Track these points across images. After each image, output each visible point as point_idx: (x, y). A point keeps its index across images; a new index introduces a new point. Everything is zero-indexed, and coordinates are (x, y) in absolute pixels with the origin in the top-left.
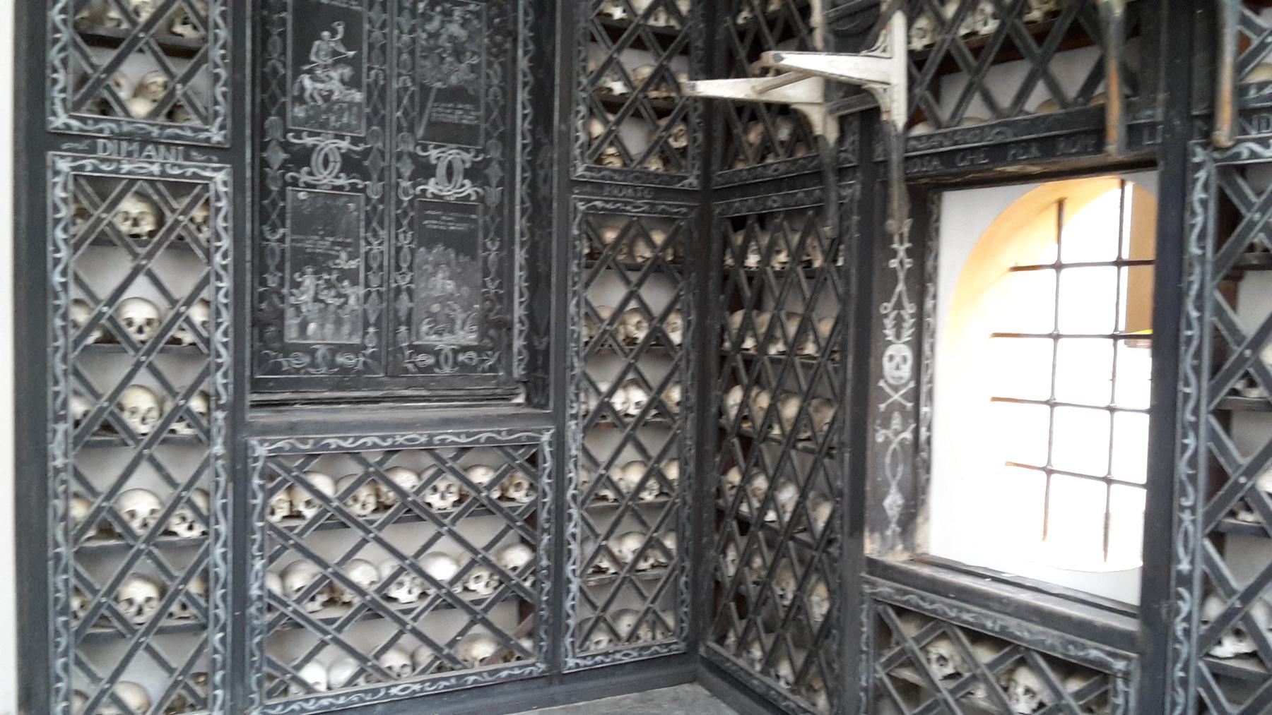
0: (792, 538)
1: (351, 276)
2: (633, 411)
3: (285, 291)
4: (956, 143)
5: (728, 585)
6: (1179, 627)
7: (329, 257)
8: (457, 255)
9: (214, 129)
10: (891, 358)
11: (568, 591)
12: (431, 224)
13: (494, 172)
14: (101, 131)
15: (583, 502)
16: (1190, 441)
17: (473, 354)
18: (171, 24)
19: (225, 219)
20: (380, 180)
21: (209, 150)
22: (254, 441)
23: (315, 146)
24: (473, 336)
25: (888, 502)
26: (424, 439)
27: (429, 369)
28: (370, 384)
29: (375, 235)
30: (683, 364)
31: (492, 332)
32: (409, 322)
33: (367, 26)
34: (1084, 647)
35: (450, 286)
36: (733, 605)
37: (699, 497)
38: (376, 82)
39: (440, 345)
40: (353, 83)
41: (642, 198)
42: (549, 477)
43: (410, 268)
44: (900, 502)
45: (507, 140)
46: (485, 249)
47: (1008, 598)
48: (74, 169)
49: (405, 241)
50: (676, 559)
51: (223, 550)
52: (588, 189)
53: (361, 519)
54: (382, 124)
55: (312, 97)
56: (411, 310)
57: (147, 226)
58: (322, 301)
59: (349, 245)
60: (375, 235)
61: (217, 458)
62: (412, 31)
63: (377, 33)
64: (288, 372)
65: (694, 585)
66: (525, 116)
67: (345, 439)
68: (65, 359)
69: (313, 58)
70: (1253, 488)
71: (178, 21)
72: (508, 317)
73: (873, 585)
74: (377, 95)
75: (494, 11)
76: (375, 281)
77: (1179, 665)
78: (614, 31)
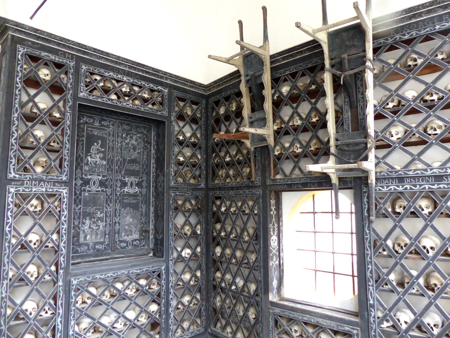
0: (242, 295)
1: (101, 219)
2: (187, 256)
3: (80, 226)
4: (292, 181)
5: (218, 310)
6: (372, 320)
7: (94, 213)
8: (133, 211)
9: (64, 176)
10: (272, 240)
11: (170, 317)
12: (126, 201)
13: (144, 184)
14: (27, 178)
15: (174, 287)
16: (370, 266)
17: (138, 241)
18: (50, 142)
19: (66, 205)
20: (110, 188)
21: (62, 183)
22: (72, 279)
23: (91, 178)
24: (138, 236)
25: (273, 283)
26: (126, 272)
27: (124, 247)
28: (106, 254)
29: (109, 205)
30: (201, 241)
31: (144, 234)
32: (118, 233)
33: (108, 141)
34: (343, 327)
35: (131, 220)
36: (220, 316)
37: (208, 281)
38: (110, 158)
39: (128, 240)
40: (103, 159)
41: (189, 191)
42: (164, 280)
43: (119, 215)
44: (277, 282)
45: (148, 174)
46: (142, 208)
47: (317, 312)
48: (15, 191)
49: (118, 207)
50: (200, 302)
51: (61, 319)
52: (174, 189)
53: (106, 302)
54: (112, 171)
55: (90, 163)
56: (119, 229)
57: (39, 208)
58: (92, 228)
59: (101, 209)
60: (109, 205)
61: (60, 286)
62: (121, 142)
63: (111, 143)
64: (80, 253)
65: (207, 310)
66: (153, 167)
67: (102, 275)
68: (8, 257)
69: (91, 151)
70: (389, 279)
71: (52, 142)
72: (148, 229)
73: (273, 310)
74: (110, 162)
75: (145, 136)
76: (108, 220)
77: (373, 331)
78: (181, 143)
